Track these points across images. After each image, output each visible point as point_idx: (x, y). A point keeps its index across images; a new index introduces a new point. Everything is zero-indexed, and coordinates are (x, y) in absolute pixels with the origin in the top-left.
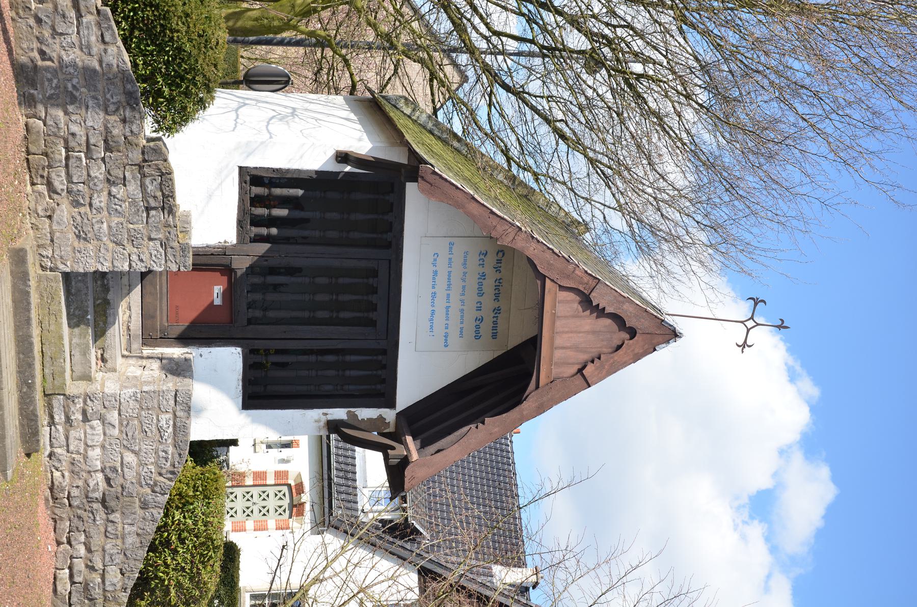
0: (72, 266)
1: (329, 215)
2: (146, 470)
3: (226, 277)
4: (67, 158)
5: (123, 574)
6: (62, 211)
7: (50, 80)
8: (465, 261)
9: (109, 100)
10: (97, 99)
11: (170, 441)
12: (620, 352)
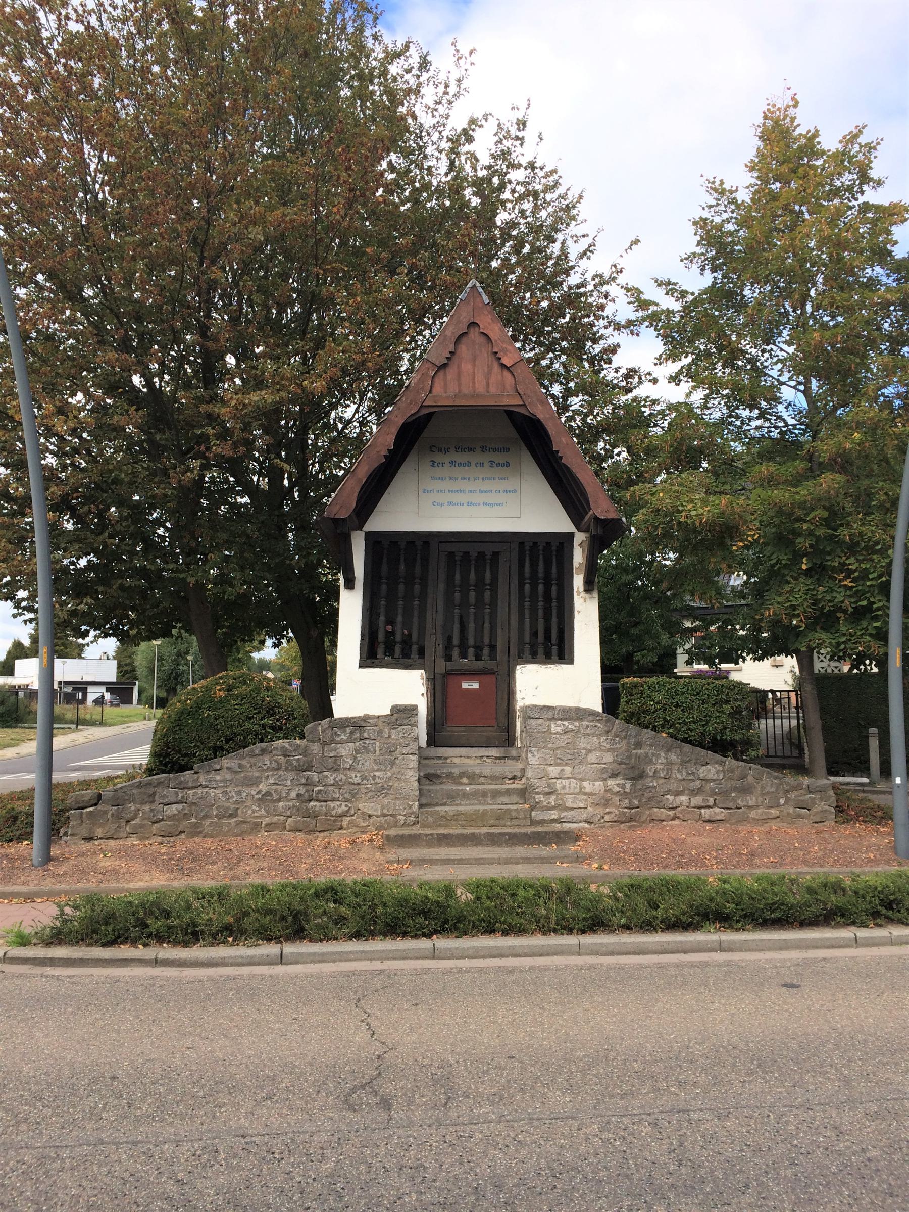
0: (414, 801)
1: (401, 594)
2: (604, 744)
3: (115, 680)
4: (318, 800)
5: (707, 764)
6: (364, 807)
7: (254, 811)
8: (439, 478)
9: (268, 767)
10: (268, 776)
11: (577, 724)
12: (491, 335)
